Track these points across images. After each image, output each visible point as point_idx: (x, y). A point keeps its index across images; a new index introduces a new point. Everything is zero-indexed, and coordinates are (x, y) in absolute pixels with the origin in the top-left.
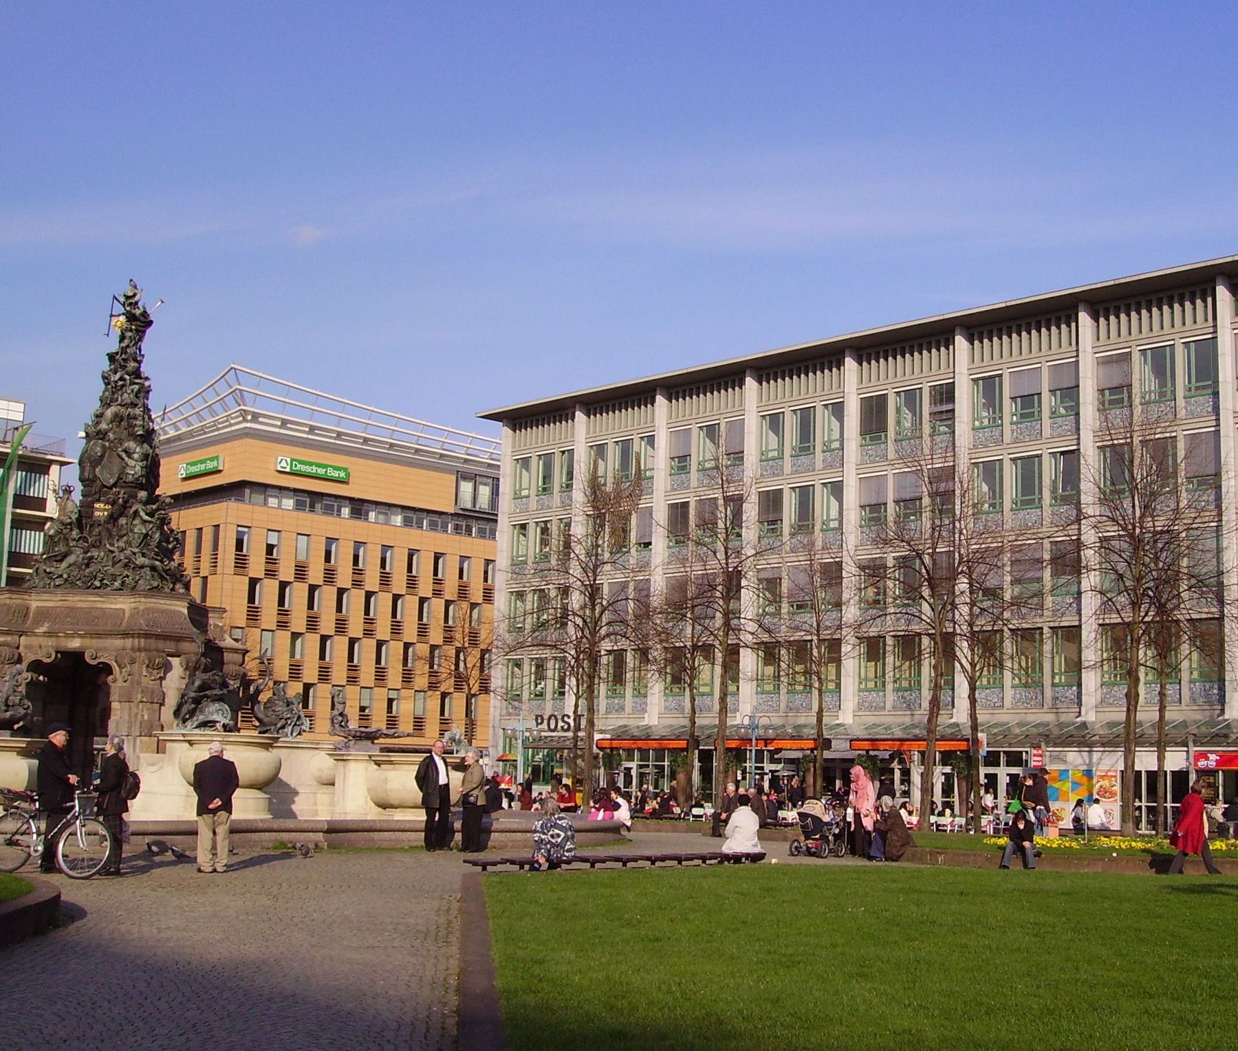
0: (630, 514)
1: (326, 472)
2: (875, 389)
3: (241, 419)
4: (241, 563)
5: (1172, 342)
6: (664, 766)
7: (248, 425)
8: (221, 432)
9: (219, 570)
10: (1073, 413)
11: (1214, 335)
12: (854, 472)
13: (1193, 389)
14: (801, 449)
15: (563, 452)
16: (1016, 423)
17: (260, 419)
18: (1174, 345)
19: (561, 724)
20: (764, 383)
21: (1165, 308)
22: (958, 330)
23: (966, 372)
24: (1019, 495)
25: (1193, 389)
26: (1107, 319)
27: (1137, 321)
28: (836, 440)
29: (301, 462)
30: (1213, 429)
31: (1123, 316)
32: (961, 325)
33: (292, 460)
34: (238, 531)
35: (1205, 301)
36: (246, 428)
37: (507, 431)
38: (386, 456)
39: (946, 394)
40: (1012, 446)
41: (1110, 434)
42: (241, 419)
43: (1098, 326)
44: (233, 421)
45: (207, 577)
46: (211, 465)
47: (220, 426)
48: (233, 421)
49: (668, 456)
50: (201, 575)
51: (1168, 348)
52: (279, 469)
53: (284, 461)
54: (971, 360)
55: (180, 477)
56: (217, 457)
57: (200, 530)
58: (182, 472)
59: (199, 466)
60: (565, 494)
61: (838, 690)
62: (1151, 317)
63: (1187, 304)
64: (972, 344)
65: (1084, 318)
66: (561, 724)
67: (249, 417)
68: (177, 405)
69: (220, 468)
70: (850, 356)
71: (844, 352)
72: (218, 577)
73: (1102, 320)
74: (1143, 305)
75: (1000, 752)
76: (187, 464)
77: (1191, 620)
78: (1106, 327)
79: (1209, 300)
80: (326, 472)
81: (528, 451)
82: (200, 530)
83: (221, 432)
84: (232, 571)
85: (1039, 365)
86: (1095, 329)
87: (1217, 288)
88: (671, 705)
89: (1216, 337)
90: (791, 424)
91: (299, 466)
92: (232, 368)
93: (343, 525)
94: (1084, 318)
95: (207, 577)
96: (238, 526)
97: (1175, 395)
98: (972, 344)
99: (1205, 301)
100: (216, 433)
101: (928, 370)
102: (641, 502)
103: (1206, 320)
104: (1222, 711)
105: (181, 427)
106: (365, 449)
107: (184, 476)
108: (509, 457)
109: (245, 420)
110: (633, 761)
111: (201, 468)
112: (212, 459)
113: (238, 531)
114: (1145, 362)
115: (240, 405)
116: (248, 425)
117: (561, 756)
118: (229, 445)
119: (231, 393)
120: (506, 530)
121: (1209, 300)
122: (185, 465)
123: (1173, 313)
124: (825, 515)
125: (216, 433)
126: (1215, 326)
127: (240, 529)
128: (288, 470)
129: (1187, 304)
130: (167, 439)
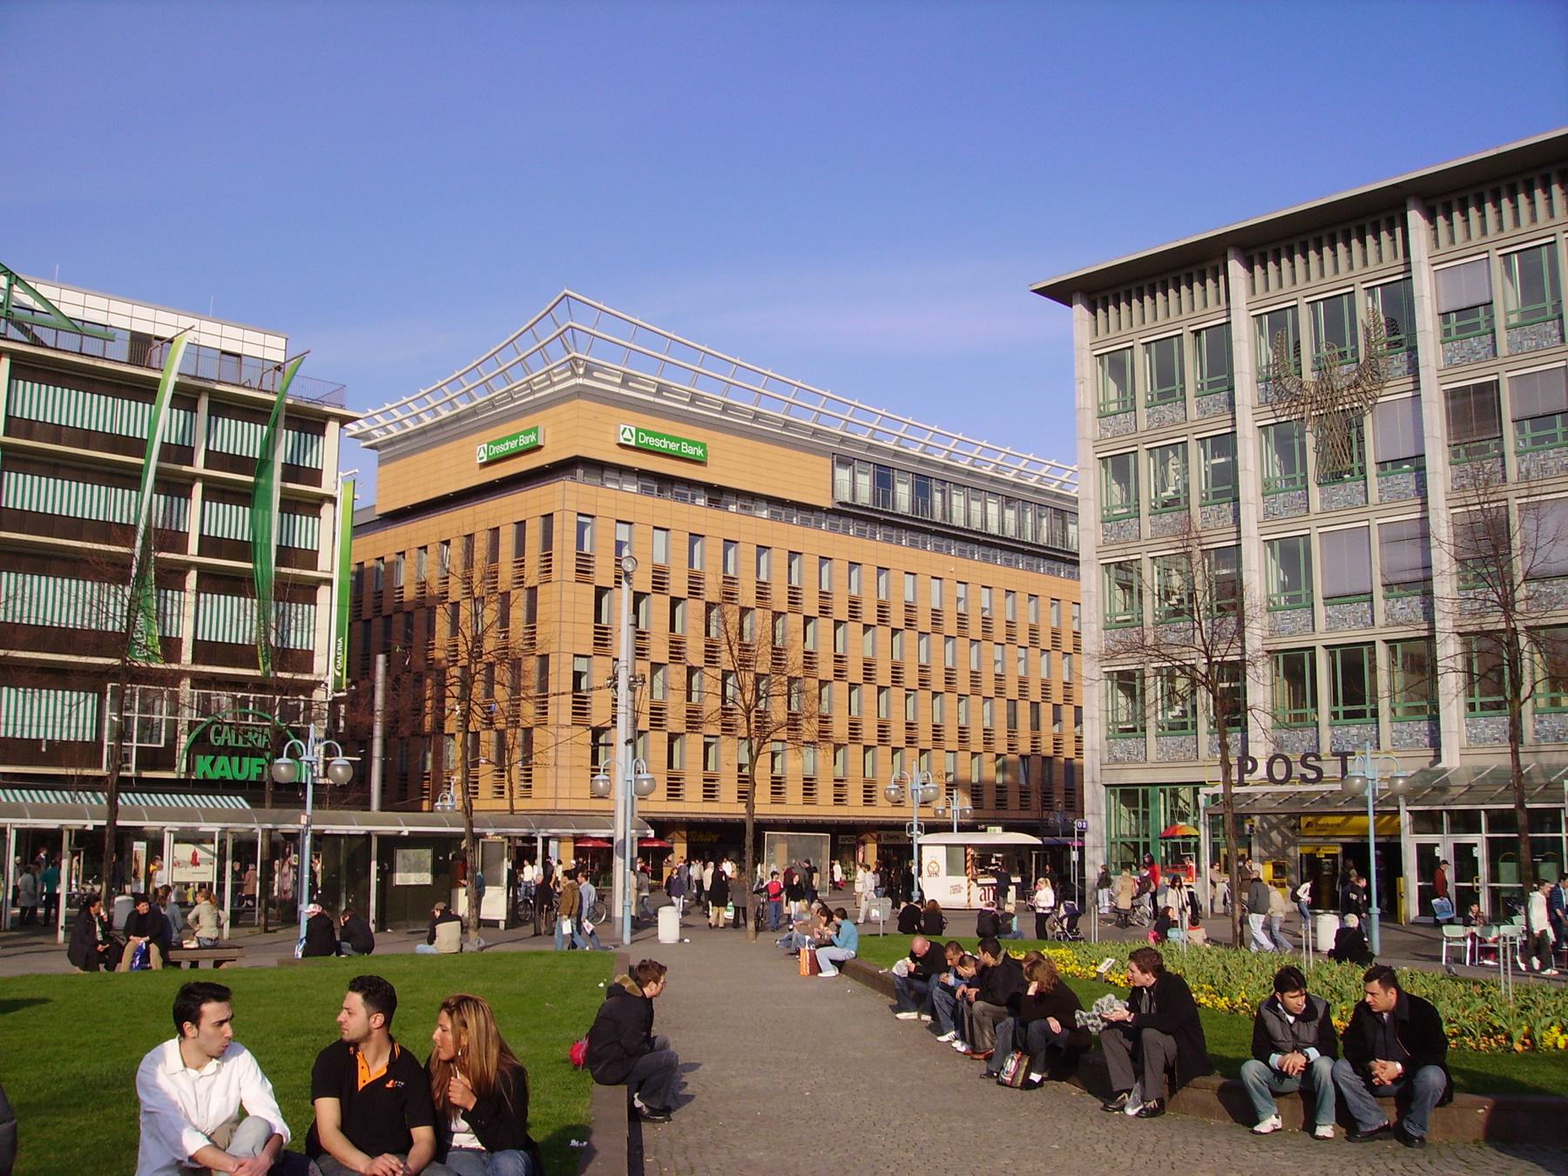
0: (1364, 414)
1: (680, 447)
2: (1151, 332)
3: (569, 373)
4: (584, 567)
5: (1351, 289)
6: (1561, 838)
7: (580, 381)
8: (537, 395)
9: (554, 576)
10: (1226, 388)
11: (1407, 275)
12: (1435, 381)
13: (1453, 331)
14: (1161, 396)
15: (1197, 333)
16: (1515, 327)
17: (595, 374)
18: (1353, 292)
19: (1298, 769)
20: (1100, 311)
21: (1489, 207)
22: (1410, 203)
23: (1244, 307)
24: (1210, 485)
25: (1453, 331)
26: (1178, 291)
27: (1263, 277)
28: (1114, 402)
29: (649, 433)
30: (1410, 394)
31: (1473, 212)
32: (1233, 246)
33: (638, 430)
34: (578, 522)
35: (1216, 281)
36: (576, 385)
37: (1079, 311)
38: (718, 422)
39: (1218, 343)
40: (1199, 423)
41: (1273, 410)
42: (569, 373)
43: (1253, 277)
44: (555, 379)
45: (535, 588)
46: (525, 441)
47: (535, 388)
48: (555, 379)
49: (1436, 312)
50: (526, 585)
51: (1345, 297)
52: (622, 441)
53: (627, 431)
54: (1094, 332)
55: (479, 461)
56: (535, 429)
57: (470, 537)
58: (482, 454)
59: (507, 444)
60: (1205, 399)
61: (1374, 719)
62: (1293, 266)
63: (1284, 262)
64: (1095, 314)
65: (1235, 268)
66: (1298, 769)
67: (581, 371)
68: (474, 364)
69: (540, 443)
70: (1416, 208)
71: (1226, 254)
72: (554, 587)
73: (1257, 268)
74: (1170, 283)
75: (1480, 810)
76: (489, 444)
77: (1528, 628)
78: (1128, 313)
79: (1398, 231)
80: (680, 447)
81: (1127, 338)
82: (470, 537)
83: (537, 395)
84: (572, 576)
85: (1485, 255)
86: (1250, 281)
87: (1409, 213)
88: (1483, 732)
89: (1411, 278)
90: (1142, 367)
91: (646, 438)
92: (566, 295)
93: (697, 513)
94: (1235, 268)
95: (535, 588)
96: (579, 514)
97: (1493, 324)
98: (1095, 314)
99: (1216, 281)
100: (531, 398)
101: (1105, 332)
102: (1385, 392)
103: (1396, 256)
104: (1438, 758)
105: (476, 396)
106: (690, 412)
107: (485, 460)
108: (1088, 352)
109: (575, 375)
110: (1480, 832)
111: (511, 446)
112: (526, 433)
113: (578, 522)
114: (1261, 332)
115: (569, 353)
116: (580, 381)
117: (1251, 826)
118: (551, 411)
119: (559, 335)
120: (1091, 467)
121: (1398, 231)
122: (485, 446)
123: (1293, 266)
124: (1105, 502)
125: (531, 398)
126: (1228, 309)
127: (582, 519)
128: (633, 443)
129: (1326, 251)
130: (422, 428)
